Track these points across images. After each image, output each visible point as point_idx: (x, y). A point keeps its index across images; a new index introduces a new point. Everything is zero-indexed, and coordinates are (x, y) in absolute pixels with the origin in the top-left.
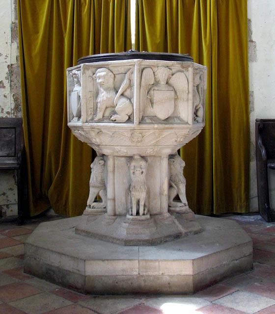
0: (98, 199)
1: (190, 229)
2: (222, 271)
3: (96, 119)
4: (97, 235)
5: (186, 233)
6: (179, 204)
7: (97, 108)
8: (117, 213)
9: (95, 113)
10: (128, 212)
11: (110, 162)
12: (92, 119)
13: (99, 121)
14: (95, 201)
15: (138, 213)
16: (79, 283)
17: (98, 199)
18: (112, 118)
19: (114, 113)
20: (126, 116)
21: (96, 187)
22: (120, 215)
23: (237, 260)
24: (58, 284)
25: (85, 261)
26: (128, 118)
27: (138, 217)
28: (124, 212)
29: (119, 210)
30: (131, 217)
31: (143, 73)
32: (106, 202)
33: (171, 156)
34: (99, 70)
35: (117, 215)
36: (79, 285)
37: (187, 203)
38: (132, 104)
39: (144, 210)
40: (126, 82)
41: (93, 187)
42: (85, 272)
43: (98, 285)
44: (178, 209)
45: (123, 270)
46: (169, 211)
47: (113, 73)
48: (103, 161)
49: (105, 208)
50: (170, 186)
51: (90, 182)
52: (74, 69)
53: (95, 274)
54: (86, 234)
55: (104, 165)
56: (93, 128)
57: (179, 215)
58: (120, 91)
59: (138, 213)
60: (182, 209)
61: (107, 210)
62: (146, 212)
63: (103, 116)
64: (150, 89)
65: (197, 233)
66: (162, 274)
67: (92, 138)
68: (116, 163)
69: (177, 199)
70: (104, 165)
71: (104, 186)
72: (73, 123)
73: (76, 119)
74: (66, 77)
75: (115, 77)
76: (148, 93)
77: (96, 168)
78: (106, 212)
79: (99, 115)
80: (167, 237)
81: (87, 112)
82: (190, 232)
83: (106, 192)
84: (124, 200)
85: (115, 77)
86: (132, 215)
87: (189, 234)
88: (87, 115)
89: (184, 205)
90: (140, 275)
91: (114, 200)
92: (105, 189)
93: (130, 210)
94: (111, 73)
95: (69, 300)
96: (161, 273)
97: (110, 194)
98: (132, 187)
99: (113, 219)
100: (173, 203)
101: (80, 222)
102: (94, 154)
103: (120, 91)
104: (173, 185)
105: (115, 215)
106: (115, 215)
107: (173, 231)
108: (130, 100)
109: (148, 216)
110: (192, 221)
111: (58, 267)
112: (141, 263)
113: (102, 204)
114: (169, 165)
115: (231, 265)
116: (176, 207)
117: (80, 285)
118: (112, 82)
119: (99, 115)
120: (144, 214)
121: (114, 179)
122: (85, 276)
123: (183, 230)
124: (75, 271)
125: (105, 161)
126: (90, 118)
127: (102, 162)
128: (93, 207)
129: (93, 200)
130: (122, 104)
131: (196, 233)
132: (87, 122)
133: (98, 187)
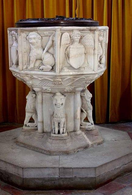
0: (31, 120)
1: (95, 142)
2: (115, 173)
3: (29, 68)
4: (32, 146)
5: (92, 144)
6: (88, 124)
7: (30, 60)
8: (45, 131)
9: (29, 64)
10: (52, 130)
11: (39, 97)
12: (27, 68)
13: (32, 69)
14: (29, 122)
15: (59, 132)
16: (19, 182)
17: (31, 120)
18: (40, 68)
19: (42, 64)
20: (51, 67)
21: (30, 112)
22: (47, 133)
23: (126, 164)
24: (5, 182)
25: (23, 168)
26: (51, 68)
27: (59, 135)
28: (49, 130)
29: (47, 129)
30: (55, 135)
31: (62, 36)
32: (37, 123)
33: (83, 91)
34: (31, 33)
35: (45, 132)
36: (19, 184)
37: (93, 122)
38: (54, 58)
39: (63, 130)
40: (50, 43)
41: (28, 112)
42: (23, 176)
43: (32, 184)
44: (87, 127)
45: (49, 175)
46: (81, 128)
47: (40, 35)
48: (35, 95)
49: (36, 127)
50: (82, 111)
51: (26, 108)
52: (13, 30)
53: (29, 177)
54: (23, 145)
55: (36, 97)
56: (27, 74)
57: (88, 132)
58: (46, 49)
59: (59, 132)
60: (89, 127)
61: (37, 128)
62: (65, 131)
63: (34, 67)
64: (67, 47)
65: (100, 144)
66: (75, 177)
67: (27, 81)
68: (44, 97)
69: (86, 120)
70: (36, 97)
71: (35, 112)
72: (12, 68)
73: (14, 66)
74: (7, 34)
75: (42, 38)
76: (66, 50)
77: (29, 97)
78: (37, 129)
79: (32, 65)
80: (79, 148)
81: (23, 63)
82: (95, 144)
83: (37, 116)
84: (49, 122)
85: (42, 38)
86: (55, 133)
87: (94, 145)
88: (23, 65)
89: (91, 124)
90: (60, 179)
91: (43, 122)
92: (36, 114)
93: (54, 130)
94: (39, 36)
95: (13, 182)
96: (74, 176)
97: (40, 118)
98: (54, 114)
99: (42, 136)
100: (85, 123)
101: (19, 133)
102: (29, 90)
103: (46, 49)
104: (84, 110)
105: (43, 132)
106: (43, 132)
107: (83, 144)
108: (53, 55)
109: (66, 134)
110: (96, 135)
111: (5, 171)
112: (60, 170)
113: (34, 124)
114: (81, 115)
115: (121, 168)
116: (86, 125)
117: (20, 184)
118: (40, 42)
119: (32, 65)
120: (63, 133)
121: (42, 108)
122: (23, 179)
123: (90, 143)
124: (17, 175)
125: (36, 95)
126: (25, 67)
127: (34, 95)
128: (28, 126)
129: (28, 121)
130: (48, 59)
131: (99, 144)
132: (22, 70)
133: (31, 112)
